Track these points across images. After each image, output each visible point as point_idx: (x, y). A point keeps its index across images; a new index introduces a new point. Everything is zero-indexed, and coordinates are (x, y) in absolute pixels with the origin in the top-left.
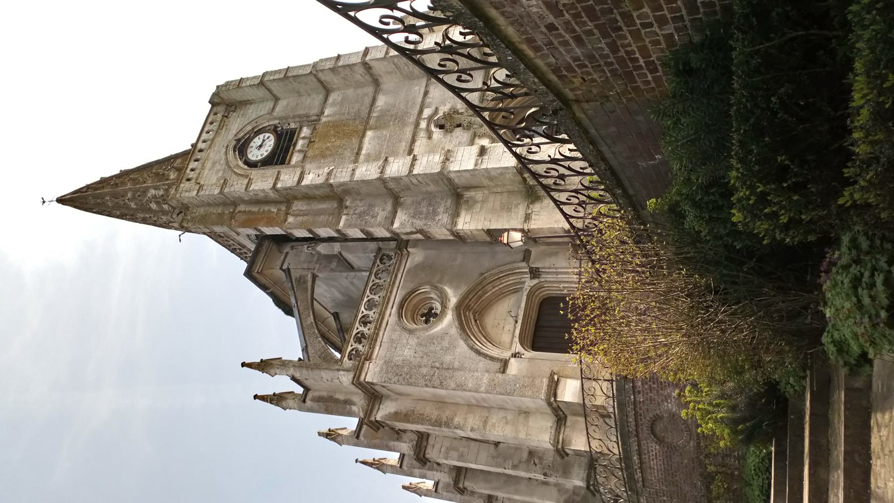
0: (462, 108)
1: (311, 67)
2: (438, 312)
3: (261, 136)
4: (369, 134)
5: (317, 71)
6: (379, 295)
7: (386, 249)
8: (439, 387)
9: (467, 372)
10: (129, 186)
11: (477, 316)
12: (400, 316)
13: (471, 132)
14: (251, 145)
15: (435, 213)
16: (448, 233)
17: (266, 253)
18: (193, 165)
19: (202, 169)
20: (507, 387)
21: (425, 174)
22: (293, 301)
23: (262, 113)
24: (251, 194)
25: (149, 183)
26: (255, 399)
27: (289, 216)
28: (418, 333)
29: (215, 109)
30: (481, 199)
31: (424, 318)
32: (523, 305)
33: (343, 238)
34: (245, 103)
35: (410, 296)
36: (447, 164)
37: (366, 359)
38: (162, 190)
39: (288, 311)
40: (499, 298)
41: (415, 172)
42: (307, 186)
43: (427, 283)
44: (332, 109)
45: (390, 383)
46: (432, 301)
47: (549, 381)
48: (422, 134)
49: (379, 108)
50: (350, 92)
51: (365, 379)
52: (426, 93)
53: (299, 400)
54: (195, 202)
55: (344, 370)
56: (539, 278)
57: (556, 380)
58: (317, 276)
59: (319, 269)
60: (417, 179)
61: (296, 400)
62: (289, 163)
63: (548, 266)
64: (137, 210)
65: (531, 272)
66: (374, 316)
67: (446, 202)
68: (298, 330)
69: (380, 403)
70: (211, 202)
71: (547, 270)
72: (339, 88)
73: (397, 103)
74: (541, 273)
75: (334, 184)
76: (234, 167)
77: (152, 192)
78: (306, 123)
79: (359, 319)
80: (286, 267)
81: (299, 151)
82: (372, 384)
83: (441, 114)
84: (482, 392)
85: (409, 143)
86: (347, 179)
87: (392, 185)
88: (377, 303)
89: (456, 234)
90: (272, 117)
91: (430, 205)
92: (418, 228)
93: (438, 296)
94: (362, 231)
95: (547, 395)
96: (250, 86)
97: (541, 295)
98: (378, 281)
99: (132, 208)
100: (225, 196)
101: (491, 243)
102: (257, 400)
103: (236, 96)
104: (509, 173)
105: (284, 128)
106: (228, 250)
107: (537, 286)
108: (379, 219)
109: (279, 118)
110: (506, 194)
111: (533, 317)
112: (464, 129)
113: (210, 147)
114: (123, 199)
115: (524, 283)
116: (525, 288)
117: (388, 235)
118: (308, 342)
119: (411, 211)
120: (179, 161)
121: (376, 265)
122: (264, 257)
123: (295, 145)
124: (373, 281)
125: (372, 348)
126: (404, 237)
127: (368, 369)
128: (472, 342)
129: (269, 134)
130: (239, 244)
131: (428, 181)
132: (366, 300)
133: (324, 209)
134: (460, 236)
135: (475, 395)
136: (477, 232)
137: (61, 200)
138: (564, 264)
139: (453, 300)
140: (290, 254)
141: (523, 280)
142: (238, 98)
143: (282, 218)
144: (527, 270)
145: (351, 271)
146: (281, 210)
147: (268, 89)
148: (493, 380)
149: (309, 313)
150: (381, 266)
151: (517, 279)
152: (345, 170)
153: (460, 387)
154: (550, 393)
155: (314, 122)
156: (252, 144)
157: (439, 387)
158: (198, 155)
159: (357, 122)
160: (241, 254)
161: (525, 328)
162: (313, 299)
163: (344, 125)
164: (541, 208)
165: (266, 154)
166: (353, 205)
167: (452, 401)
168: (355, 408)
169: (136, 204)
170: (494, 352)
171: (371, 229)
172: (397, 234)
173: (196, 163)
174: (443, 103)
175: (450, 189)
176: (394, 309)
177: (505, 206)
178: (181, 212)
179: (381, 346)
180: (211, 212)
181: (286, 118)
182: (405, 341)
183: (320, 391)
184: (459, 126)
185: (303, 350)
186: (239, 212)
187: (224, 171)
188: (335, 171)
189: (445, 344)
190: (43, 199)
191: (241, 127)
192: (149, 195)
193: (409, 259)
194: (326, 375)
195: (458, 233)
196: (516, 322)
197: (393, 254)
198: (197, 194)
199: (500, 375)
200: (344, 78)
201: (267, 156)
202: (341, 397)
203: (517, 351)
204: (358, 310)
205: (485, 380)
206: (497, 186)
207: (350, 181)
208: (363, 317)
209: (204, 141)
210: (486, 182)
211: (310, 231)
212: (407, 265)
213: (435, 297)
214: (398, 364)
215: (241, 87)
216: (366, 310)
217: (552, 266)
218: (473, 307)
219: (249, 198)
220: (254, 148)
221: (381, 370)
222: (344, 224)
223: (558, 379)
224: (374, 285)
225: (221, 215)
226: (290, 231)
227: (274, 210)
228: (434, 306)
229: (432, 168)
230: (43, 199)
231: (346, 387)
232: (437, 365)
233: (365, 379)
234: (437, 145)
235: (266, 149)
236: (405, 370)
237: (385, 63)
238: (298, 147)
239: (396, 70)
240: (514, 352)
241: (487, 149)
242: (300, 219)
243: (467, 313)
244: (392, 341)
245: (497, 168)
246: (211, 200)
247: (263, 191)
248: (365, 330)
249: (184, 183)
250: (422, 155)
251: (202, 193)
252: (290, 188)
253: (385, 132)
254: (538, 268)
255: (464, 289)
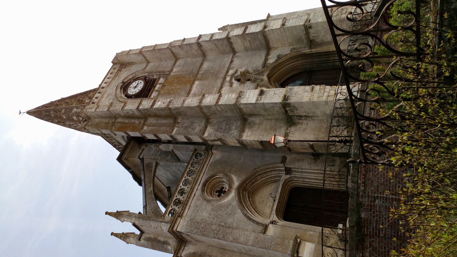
0: (252, 71)
1: (169, 44)
2: (226, 190)
3: (137, 82)
4: (197, 82)
5: (171, 47)
6: (192, 177)
7: (200, 150)
8: (222, 239)
9: (241, 230)
10: (64, 106)
11: (250, 195)
12: (203, 190)
13: (256, 83)
14: (130, 86)
15: (230, 129)
16: (236, 142)
17: (131, 148)
18: (97, 95)
19: (102, 98)
20: (266, 243)
21: (226, 105)
22: (142, 177)
23: (139, 69)
24: (125, 112)
25: (74, 105)
26: (111, 235)
27: (145, 126)
28: (213, 203)
29: (114, 66)
30: (258, 122)
31: (218, 194)
32: (280, 190)
33: (173, 141)
34: (131, 64)
35: (210, 179)
36: (239, 99)
37: (179, 216)
38: (80, 109)
39: (140, 182)
40: (265, 184)
41: (220, 103)
42: (156, 109)
43: (221, 172)
44: (177, 68)
45: (192, 233)
46: (224, 184)
47: (294, 242)
48: (227, 84)
49: (204, 69)
50: (189, 60)
51: (177, 229)
52: (232, 62)
53: (137, 238)
54: (94, 115)
55: (164, 222)
56: (291, 174)
57: (299, 242)
58: (159, 164)
59: (160, 160)
60: (220, 107)
61: (135, 238)
62: (150, 97)
63: (297, 168)
64: (65, 119)
65: (286, 170)
66: (187, 189)
67: (237, 123)
68: (143, 194)
69: (185, 246)
70: (103, 116)
71: (296, 170)
72: (183, 57)
73: (215, 66)
74: (292, 171)
75: (172, 108)
76: (119, 97)
77: (75, 110)
78: (163, 76)
79: (178, 190)
80: (142, 157)
81: (157, 91)
82: (181, 232)
83: (239, 73)
84: (249, 245)
85: (219, 89)
86: (180, 105)
87: (205, 111)
88: (190, 182)
89: (241, 142)
90: (144, 71)
91: (227, 124)
92: (219, 137)
93: (227, 180)
94: (186, 137)
95: (292, 252)
96: (134, 54)
97: (291, 185)
98: (192, 168)
99: (64, 119)
100: (110, 112)
101: (262, 150)
102: (113, 236)
103: (126, 59)
104: (277, 107)
105: (150, 78)
106: (112, 145)
107: (289, 179)
108: (196, 131)
109: (148, 72)
110: (274, 121)
111: (285, 199)
112: (252, 82)
113: (108, 86)
114: (59, 113)
115: (281, 177)
116: (281, 180)
117: (201, 141)
118: (147, 203)
119: (216, 127)
120: (91, 94)
121: (193, 159)
122: (130, 150)
123: (155, 87)
124: (190, 168)
125: (183, 209)
126: (210, 143)
127: (179, 222)
128: (246, 211)
129: (141, 81)
130: (117, 142)
131: (227, 110)
132: (184, 179)
133: (165, 123)
134: (243, 144)
135: (245, 246)
136: (254, 142)
137: (29, 113)
138: (307, 167)
139: (236, 184)
140: (145, 150)
141: (280, 175)
142: (128, 61)
143: (141, 127)
144: (283, 169)
145: (178, 162)
146: (141, 123)
147: (144, 56)
148: (257, 238)
149: (151, 186)
150: (195, 160)
151: (277, 174)
152: (179, 100)
153: (236, 240)
154: (295, 251)
155: (166, 75)
156: (131, 86)
157: (222, 239)
158: (101, 90)
159: (191, 76)
160: (119, 148)
161: (280, 205)
162: (154, 175)
163: (183, 77)
164: (295, 130)
165: (138, 91)
166: (182, 122)
167: (229, 249)
168: (169, 247)
169: (66, 116)
170: (259, 219)
171: (191, 137)
172: (206, 141)
173: (99, 94)
174: (241, 67)
175: (240, 116)
176: (200, 186)
177: (273, 128)
178: (85, 121)
179: (189, 208)
180: (102, 122)
181: (151, 72)
182: (204, 207)
183: (150, 234)
184: (249, 80)
185: (144, 208)
186: (118, 122)
187: (113, 99)
188: (173, 100)
189: (229, 211)
190: (20, 111)
191: (127, 76)
192: (73, 112)
193: (212, 157)
194: (153, 224)
195: (242, 142)
196: (275, 201)
197: (203, 153)
198: (95, 110)
199: (262, 235)
200: (186, 52)
201: (138, 93)
202: (162, 239)
203: (274, 220)
204: (178, 185)
205: (252, 237)
206: (269, 115)
207: (181, 107)
208: (181, 189)
209: (106, 83)
210: (262, 112)
211: (156, 135)
212: (211, 160)
213: (226, 181)
214: (198, 221)
215: (129, 54)
216: (183, 185)
217: (299, 167)
218: (248, 189)
219: (124, 114)
220: (132, 88)
221: (187, 224)
222: (176, 133)
223: (300, 241)
224: (189, 171)
225: (107, 123)
226: (144, 135)
227: (137, 122)
228: (224, 186)
229: (230, 101)
230: (20, 111)
231: (165, 233)
232: (222, 224)
233: (177, 229)
234: (235, 90)
235: (138, 89)
236: (202, 225)
237: (210, 44)
238: (156, 88)
239: (216, 48)
240: (272, 220)
241: (264, 92)
242: (151, 128)
243: (244, 192)
244: (196, 206)
245: (270, 103)
246: (103, 114)
247: (132, 110)
248: (181, 198)
249: (90, 105)
250: (225, 94)
251: (98, 110)
252: (147, 109)
253: (205, 82)
254: (291, 168)
255: (243, 177)
